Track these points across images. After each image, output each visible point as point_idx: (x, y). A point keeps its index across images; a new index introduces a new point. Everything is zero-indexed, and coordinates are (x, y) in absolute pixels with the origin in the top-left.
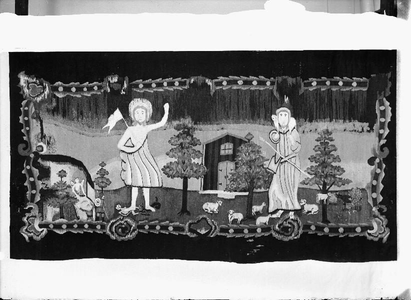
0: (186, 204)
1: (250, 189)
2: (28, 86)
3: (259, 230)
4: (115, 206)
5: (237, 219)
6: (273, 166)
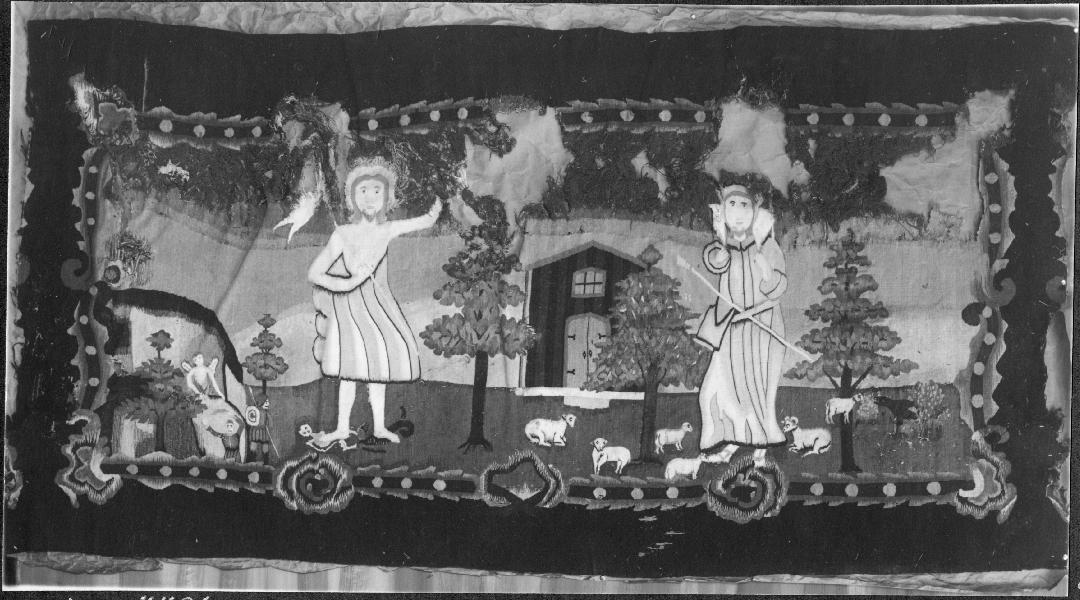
0: (482, 409)
1: (648, 385)
2: (96, 109)
3: (672, 493)
4: (298, 429)
5: (615, 463)
6: (711, 333)
